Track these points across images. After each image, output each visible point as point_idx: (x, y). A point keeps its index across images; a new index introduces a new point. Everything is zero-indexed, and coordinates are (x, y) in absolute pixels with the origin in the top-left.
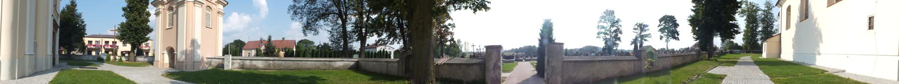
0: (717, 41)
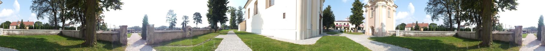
0: (219, 24)
